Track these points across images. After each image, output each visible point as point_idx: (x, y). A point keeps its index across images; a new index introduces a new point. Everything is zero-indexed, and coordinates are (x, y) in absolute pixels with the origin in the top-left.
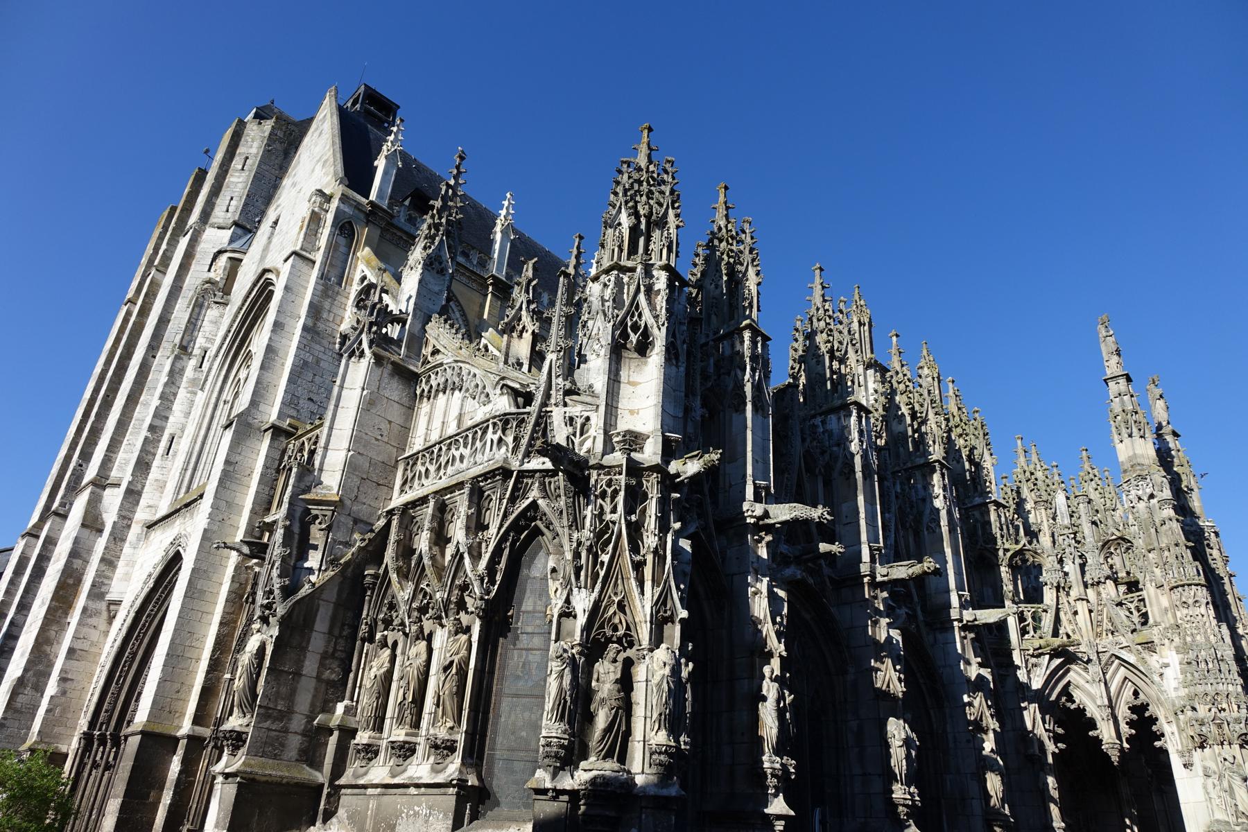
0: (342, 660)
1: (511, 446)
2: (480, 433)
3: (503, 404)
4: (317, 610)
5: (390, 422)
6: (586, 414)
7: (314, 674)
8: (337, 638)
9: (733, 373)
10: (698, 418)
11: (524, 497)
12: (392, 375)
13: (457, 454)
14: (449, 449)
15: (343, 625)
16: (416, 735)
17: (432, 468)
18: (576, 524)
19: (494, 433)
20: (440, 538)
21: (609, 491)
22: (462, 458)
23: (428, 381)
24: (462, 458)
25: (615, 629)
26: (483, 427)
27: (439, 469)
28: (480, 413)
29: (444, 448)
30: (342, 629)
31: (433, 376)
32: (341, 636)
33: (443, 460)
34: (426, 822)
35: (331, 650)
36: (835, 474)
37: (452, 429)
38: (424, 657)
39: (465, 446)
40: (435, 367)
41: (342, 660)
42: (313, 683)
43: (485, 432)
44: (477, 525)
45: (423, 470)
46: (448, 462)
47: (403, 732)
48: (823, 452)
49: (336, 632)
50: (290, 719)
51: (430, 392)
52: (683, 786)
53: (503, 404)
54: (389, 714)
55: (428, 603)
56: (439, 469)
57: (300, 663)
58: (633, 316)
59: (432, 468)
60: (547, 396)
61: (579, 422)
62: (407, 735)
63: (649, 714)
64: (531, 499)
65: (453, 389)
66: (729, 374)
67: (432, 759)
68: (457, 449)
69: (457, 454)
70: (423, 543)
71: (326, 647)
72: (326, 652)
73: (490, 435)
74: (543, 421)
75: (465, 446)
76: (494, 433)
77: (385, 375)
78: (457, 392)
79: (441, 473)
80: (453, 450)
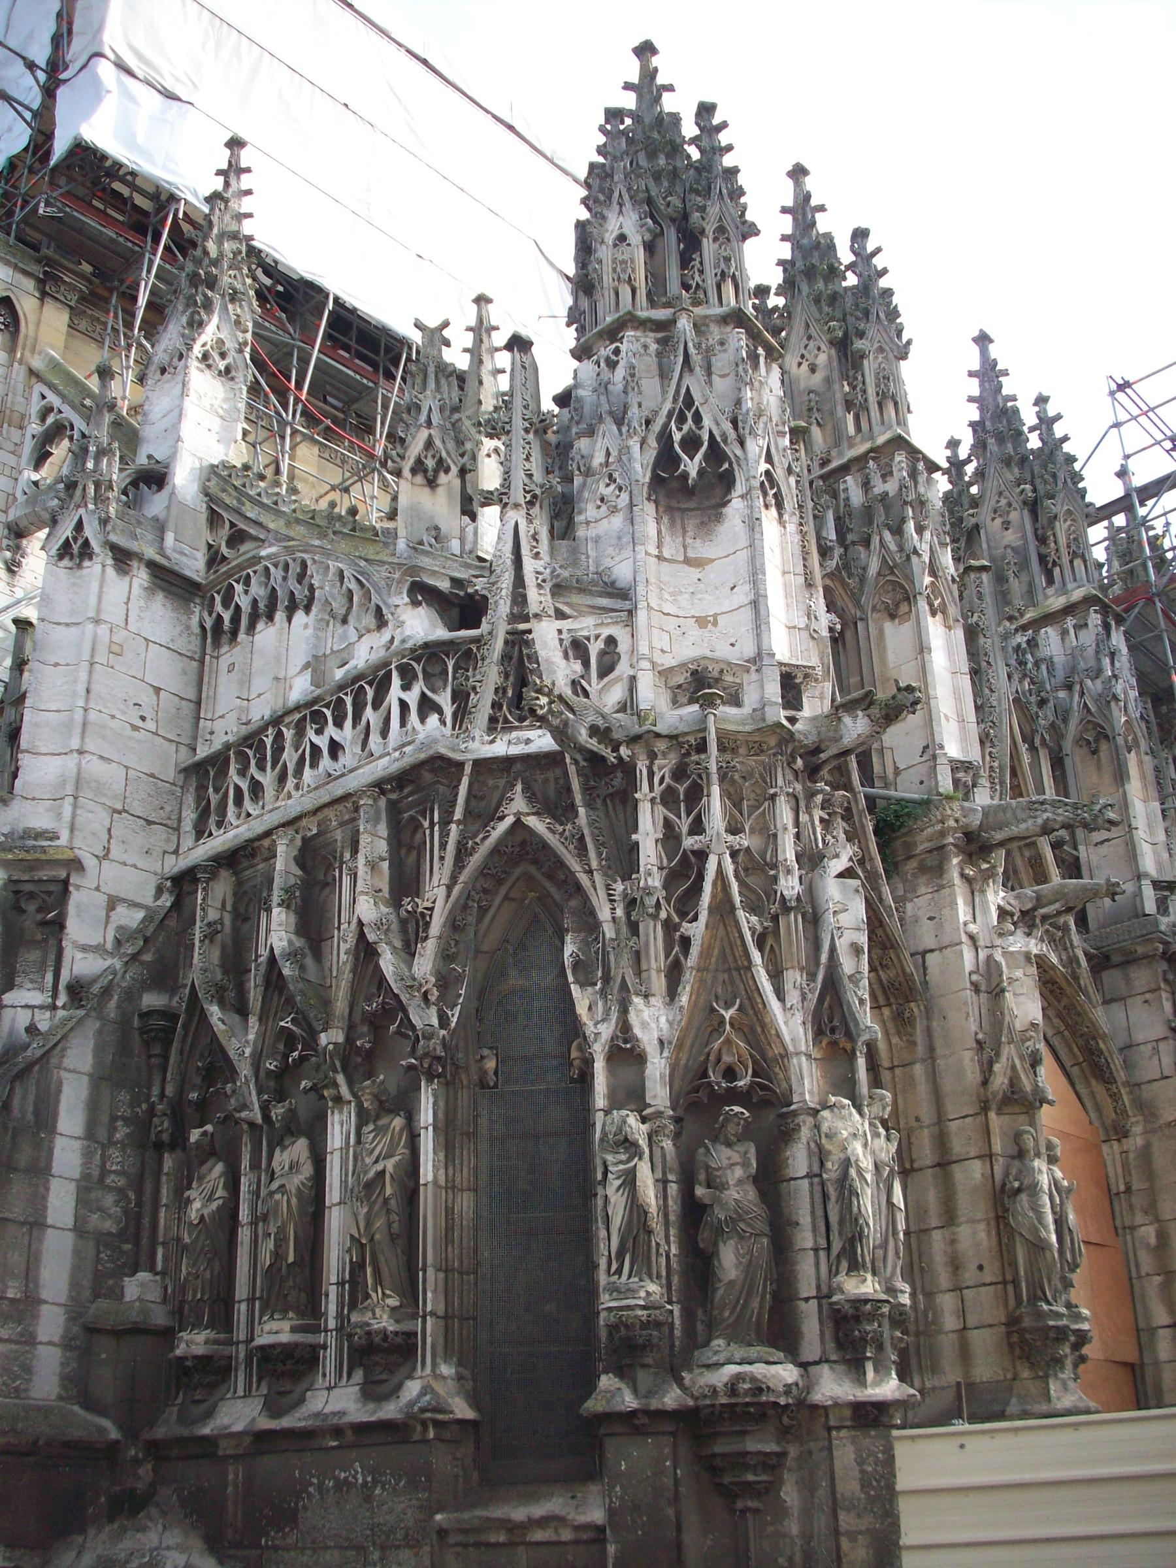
0: (121, 1191)
1: (448, 710)
2: (370, 693)
3: (420, 625)
4: (59, 1091)
5: (157, 690)
6: (606, 632)
7: (70, 1225)
8: (104, 1148)
9: (876, 540)
10: (825, 633)
11: (495, 816)
12: (150, 591)
13: (322, 742)
14: (300, 732)
15: (114, 1119)
16: (315, 1329)
17: (267, 779)
18: (625, 861)
19: (406, 687)
20: (313, 925)
21: (681, 789)
22: (335, 748)
23: (227, 601)
24: (335, 748)
25: (730, 1074)
26: (378, 679)
27: (282, 778)
28: (366, 651)
29: (289, 734)
30: (112, 1129)
31: (239, 588)
32: (111, 1143)
33: (289, 757)
34: (368, 1499)
35: (96, 1173)
36: (1068, 745)
37: (300, 688)
38: (307, 1170)
39: (339, 724)
40: (240, 567)
41: (121, 1191)
42: (69, 1239)
43: (383, 687)
44: (405, 883)
45: (244, 786)
46: (302, 759)
47: (286, 1325)
48: (1042, 703)
49: (102, 1134)
50: (35, 1317)
51: (236, 619)
52: (588, 1386)
53: (420, 625)
54: (241, 1291)
55: (302, 1059)
56: (282, 778)
57: (39, 1202)
58: (682, 419)
59: (267, 779)
60: (519, 598)
61: (595, 648)
62: (294, 1330)
63: (823, 1243)
64: (510, 820)
65: (291, 610)
66: (867, 543)
67: (358, 1376)
68: (319, 732)
69: (322, 742)
70: (278, 931)
71: (86, 1164)
72: (86, 1177)
73: (395, 691)
74: (519, 657)
75: (339, 724)
76: (406, 687)
77: (136, 591)
78: (300, 617)
79: (291, 783)
80: (311, 734)
